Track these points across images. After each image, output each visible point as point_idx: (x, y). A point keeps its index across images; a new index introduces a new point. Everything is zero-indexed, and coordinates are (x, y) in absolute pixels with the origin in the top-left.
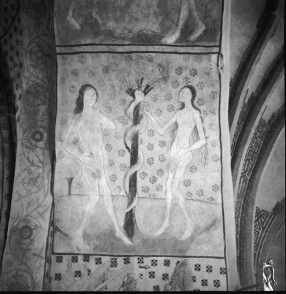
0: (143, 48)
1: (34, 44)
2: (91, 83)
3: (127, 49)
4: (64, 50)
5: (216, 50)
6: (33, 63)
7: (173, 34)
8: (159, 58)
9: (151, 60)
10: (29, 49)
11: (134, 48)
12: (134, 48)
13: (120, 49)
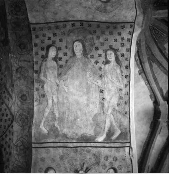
0: (84, 145)
1: (20, 141)
2: (52, 166)
3: (75, 145)
4: (37, 145)
5: (128, 145)
6: (17, 153)
7: (102, 135)
8: (95, 150)
9: (89, 152)
10: (16, 144)
11: (79, 145)
12: (79, 145)
13: (71, 145)
